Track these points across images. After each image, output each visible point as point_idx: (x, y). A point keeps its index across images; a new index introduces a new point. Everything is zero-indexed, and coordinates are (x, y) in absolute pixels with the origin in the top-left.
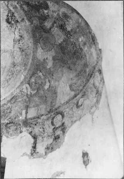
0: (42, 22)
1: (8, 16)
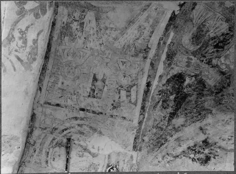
0: (208, 91)
1: (193, 160)
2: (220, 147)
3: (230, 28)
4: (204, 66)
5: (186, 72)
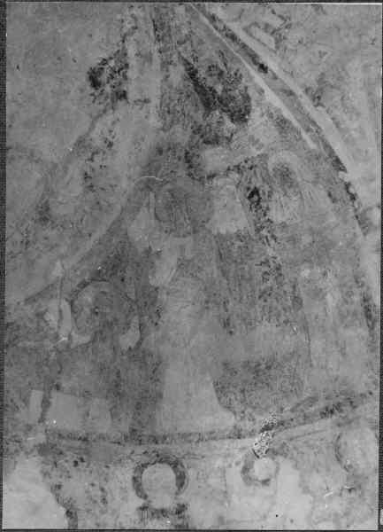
1: (105, 62)
2: (105, 111)
3: (272, 222)
4: (239, 159)
5: (245, 130)
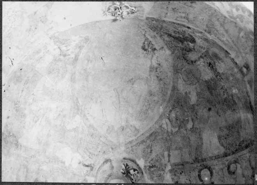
0: (185, 53)
1: (144, 43)
2: (152, 56)
3: (219, 73)
